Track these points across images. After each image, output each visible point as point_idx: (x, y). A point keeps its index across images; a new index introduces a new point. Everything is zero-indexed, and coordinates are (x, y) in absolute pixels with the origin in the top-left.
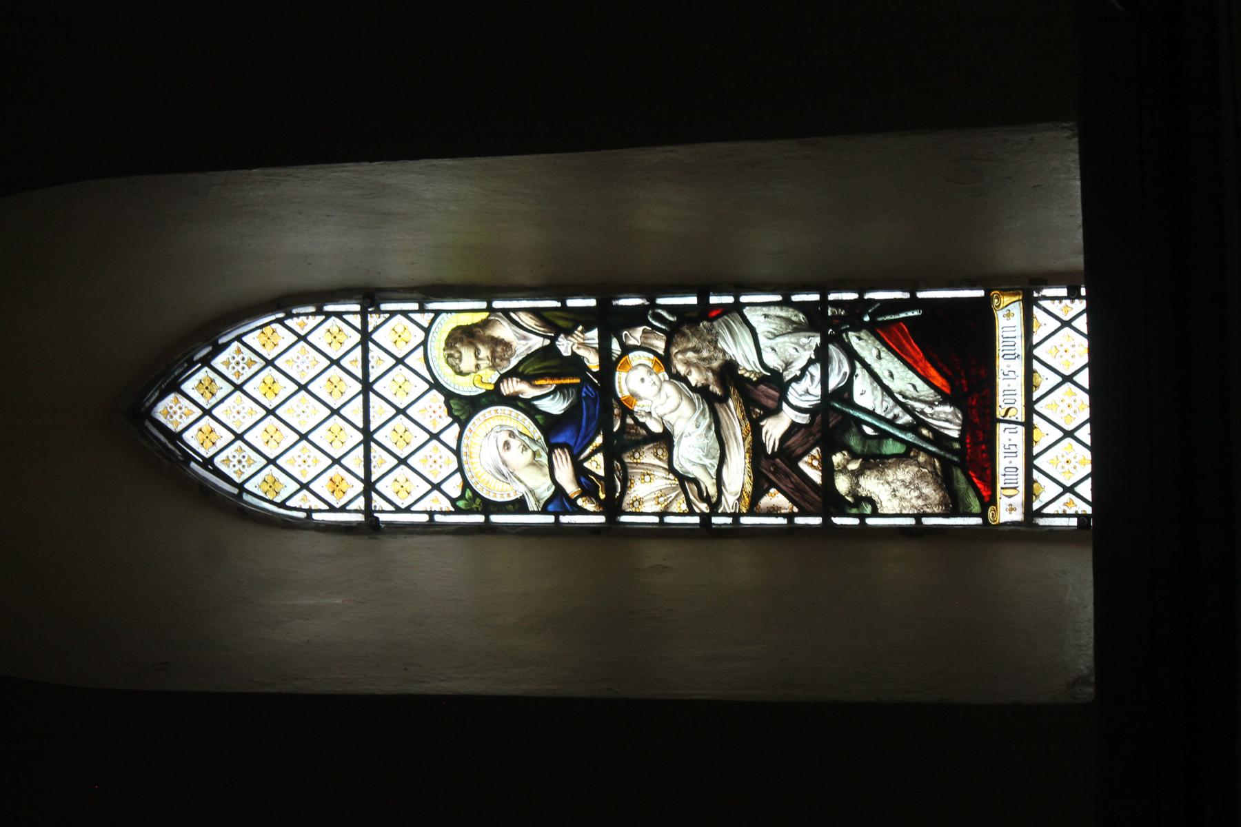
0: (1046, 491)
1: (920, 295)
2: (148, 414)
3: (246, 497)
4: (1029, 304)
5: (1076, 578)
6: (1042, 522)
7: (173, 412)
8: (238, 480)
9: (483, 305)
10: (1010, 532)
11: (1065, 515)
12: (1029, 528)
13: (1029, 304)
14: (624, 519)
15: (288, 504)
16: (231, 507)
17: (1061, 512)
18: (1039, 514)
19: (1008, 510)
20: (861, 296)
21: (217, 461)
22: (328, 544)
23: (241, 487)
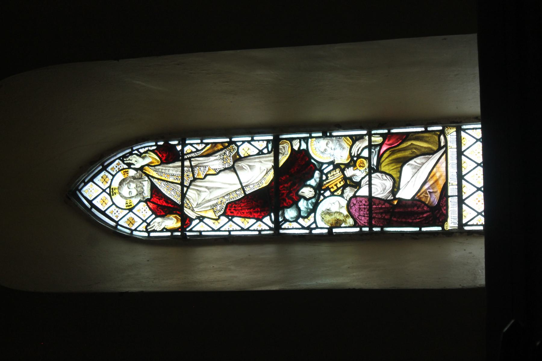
0: (468, 215)
1: (394, 131)
2: (72, 195)
3: (119, 227)
4: (459, 131)
5: (477, 251)
6: (466, 228)
7: (90, 191)
8: (117, 220)
9: (154, 144)
10: (450, 234)
11: (477, 225)
12: (461, 232)
13: (459, 131)
14: (271, 138)
15: (138, 229)
16: (113, 233)
17: (475, 224)
18: (466, 224)
19: (452, 223)
20: (389, 131)
21: (179, 182)
22: (144, 254)
23: (117, 222)
